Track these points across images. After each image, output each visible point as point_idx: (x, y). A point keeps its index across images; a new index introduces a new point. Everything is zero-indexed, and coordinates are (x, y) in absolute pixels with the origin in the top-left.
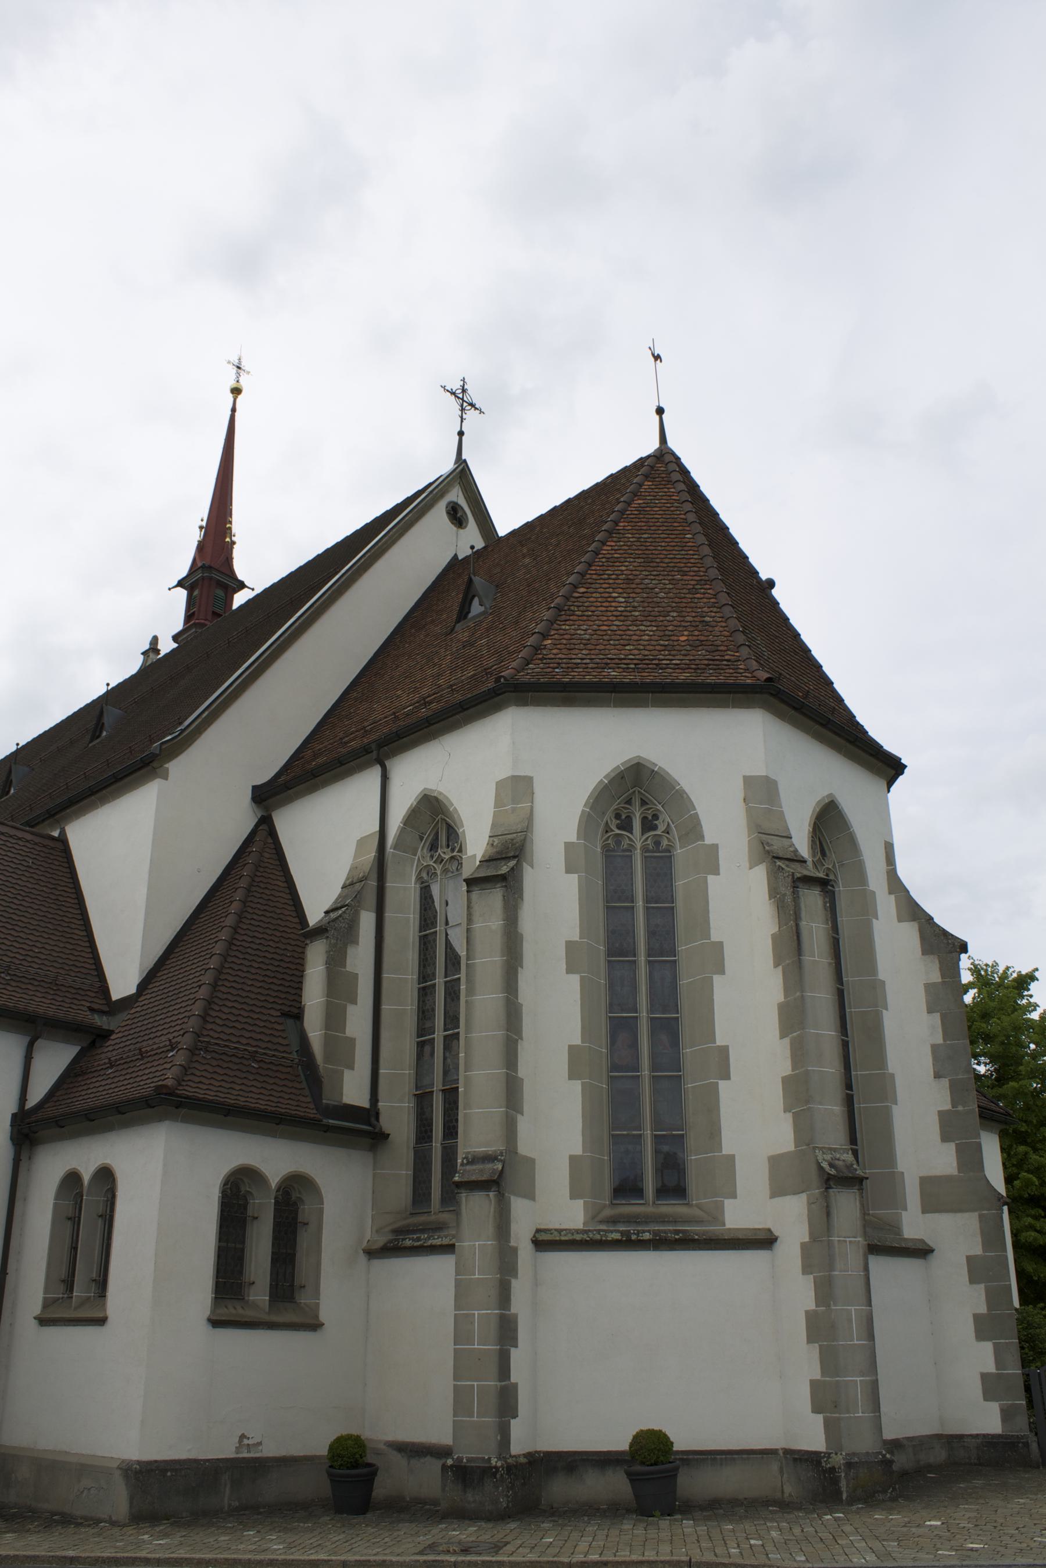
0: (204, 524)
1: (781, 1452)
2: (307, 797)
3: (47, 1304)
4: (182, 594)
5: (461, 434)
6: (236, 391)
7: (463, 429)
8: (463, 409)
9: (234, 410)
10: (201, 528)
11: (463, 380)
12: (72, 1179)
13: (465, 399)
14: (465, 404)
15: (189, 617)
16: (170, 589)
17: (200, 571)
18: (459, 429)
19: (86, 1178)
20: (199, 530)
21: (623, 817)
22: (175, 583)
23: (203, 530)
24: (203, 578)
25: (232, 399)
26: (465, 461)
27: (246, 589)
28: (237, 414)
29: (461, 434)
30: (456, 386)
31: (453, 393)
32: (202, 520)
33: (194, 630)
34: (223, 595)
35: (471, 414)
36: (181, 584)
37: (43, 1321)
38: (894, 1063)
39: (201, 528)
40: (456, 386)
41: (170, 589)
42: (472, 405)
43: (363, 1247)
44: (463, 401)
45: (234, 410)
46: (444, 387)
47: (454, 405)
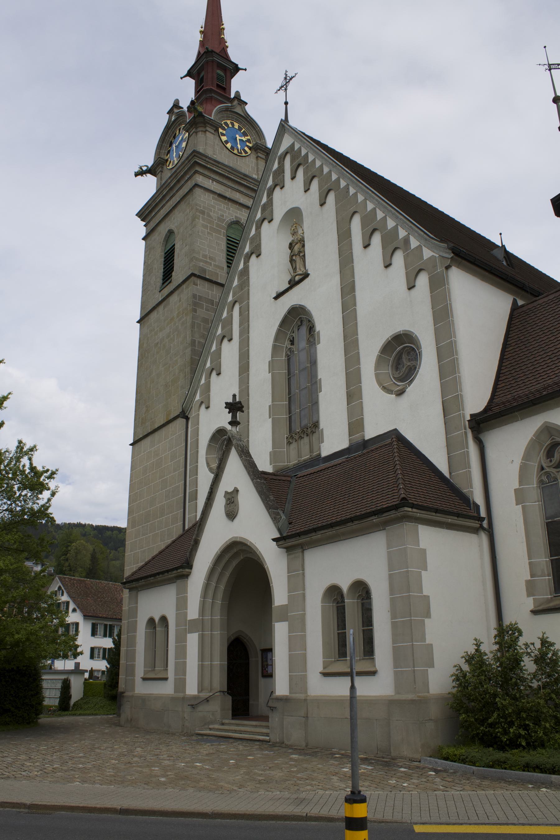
2: (503, 427)
3: (145, 672)
4: (191, 83)
5: (286, 103)
7: (287, 100)
8: (291, 79)
10: (201, 32)
12: (151, 621)
13: (285, 83)
14: (287, 81)
17: (204, 56)
18: (285, 101)
19: (157, 620)
21: (549, 460)
22: (186, 73)
24: (207, 62)
27: (240, 71)
29: (286, 103)
36: (190, 74)
37: (144, 679)
38: (269, 424)
44: (286, 83)
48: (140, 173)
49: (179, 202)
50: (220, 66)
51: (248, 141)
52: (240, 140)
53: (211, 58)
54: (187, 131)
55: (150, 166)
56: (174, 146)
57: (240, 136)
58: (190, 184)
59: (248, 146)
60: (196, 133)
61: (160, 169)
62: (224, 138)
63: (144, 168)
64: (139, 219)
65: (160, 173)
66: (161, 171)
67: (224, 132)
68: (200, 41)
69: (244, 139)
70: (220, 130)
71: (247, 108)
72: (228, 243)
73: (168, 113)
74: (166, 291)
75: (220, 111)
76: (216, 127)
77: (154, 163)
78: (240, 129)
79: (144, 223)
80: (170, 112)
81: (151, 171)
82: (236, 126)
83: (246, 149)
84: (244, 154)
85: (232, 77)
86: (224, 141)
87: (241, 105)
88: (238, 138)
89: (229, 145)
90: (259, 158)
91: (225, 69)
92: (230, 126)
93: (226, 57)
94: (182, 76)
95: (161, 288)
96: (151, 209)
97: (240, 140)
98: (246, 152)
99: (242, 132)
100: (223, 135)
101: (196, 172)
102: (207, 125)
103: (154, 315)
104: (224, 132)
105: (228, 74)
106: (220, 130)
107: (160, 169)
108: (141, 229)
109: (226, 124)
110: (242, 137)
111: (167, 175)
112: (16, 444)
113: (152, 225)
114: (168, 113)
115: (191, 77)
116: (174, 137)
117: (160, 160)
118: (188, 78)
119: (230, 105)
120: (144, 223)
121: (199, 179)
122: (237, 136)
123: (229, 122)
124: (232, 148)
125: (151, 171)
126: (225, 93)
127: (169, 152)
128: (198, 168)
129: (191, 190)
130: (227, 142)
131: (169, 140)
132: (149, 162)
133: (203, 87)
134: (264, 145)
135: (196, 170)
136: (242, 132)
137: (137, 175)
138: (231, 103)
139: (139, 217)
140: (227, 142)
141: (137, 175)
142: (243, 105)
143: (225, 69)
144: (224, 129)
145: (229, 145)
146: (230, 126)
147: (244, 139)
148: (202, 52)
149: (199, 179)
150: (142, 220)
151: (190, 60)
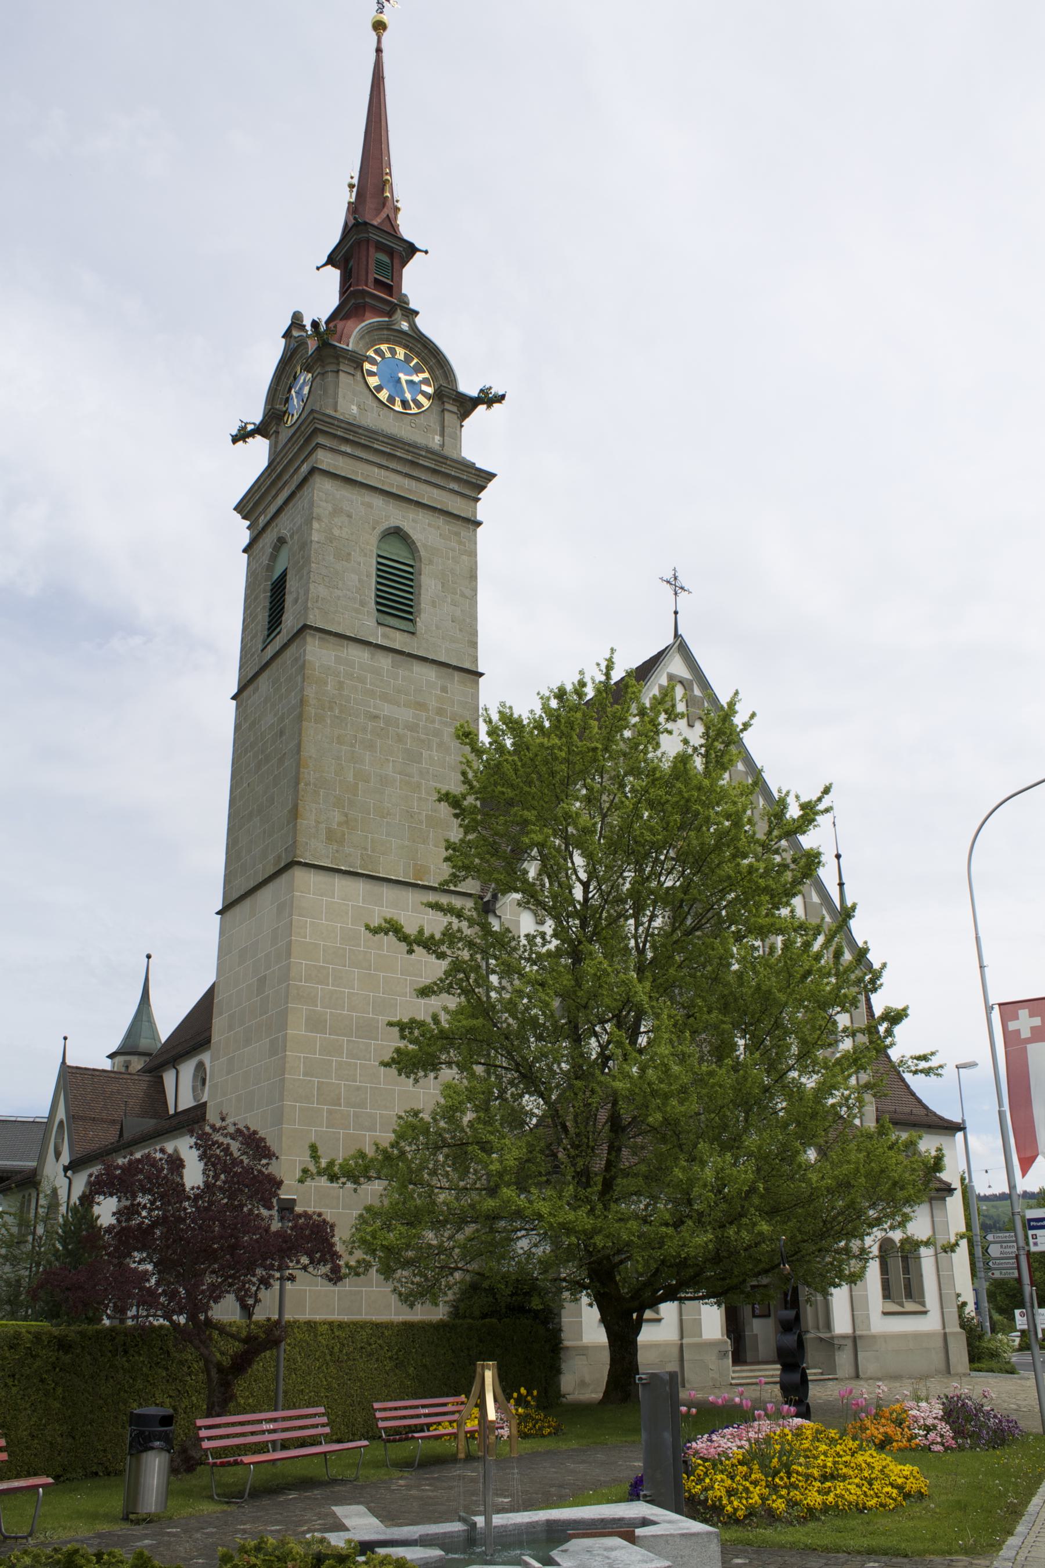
0: (355, 181)
1: (727, 1225)
4: (334, 275)
6: (379, 26)
9: (379, 50)
11: (675, 569)
15: (666, 1301)
16: (318, 268)
20: (348, 189)
22: (324, 259)
23: (355, 190)
25: (376, 38)
26: (681, 636)
28: (386, 56)
30: (669, 576)
31: (668, 582)
32: (352, 178)
33: (353, 301)
34: (388, 261)
35: (682, 595)
36: (331, 261)
39: (351, 186)
40: (669, 576)
41: (318, 268)
42: (682, 588)
43: (297, 1177)
45: (379, 50)
46: (661, 579)
47: (669, 590)
48: (242, 436)
49: (292, 495)
50: (380, 247)
51: (425, 381)
52: (407, 381)
53: (366, 235)
54: (309, 372)
55: (258, 422)
56: (293, 392)
57: (406, 374)
58: (305, 469)
59: (424, 393)
60: (323, 374)
61: (274, 429)
62: (373, 381)
63: (250, 427)
64: (239, 516)
65: (274, 436)
66: (275, 431)
67: (374, 369)
68: (349, 203)
69: (416, 378)
70: (367, 366)
71: (419, 321)
72: (379, 576)
73: (283, 337)
74: (270, 651)
75: (371, 330)
76: (357, 361)
77: (264, 417)
78: (408, 359)
79: (248, 523)
80: (287, 335)
81: (261, 430)
82: (401, 353)
83: (421, 398)
84: (415, 411)
85: (404, 264)
86: (374, 387)
87: (408, 317)
88: (403, 377)
89: (383, 395)
90: (446, 412)
91: (390, 252)
92: (388, 355)
93: (393, 233)
94: (319, 265)
95: (264, 642)
96: (265, 490)
97: (407, 381)
98: (419, 405)
99: (412, 365)
100: (371, 374)
101: (318, 445)
102: (341, 360)
103: (263, 681)
104: (374, 369)
105: (396, 261)
106: (367, 366)
107: (274, 429)
108: (241, 531)
109: (378, 352)
110: (411, 375)
111: (285, 435)
112: (501, 393)
113: (262, 521)
114: (283, 337)
115: (334, 266)
116: (295, 378)
117: (273, 413)
118: (329, 267)
119: (387, 319)
120: (248, 523)
121: (325, 459)
122: (401, 375)
123: (384, 347)
124: (391, 399)
125: (261, 430)
126: (391, 296)
127: (287, 400)
128: (321, 440)
129: (305, 480)
130: (379, 388)
131: (287, 383)
132: (256, 416)
133: (350, 286)
134: (454, 388)
135: (318, 444)
136: (412, 365)
137: (235, 440)
138: (390, 317)
139: (238, 512)
140: (379, 388)
141: (235, 440)
142: (411, 317)
143: (390, 252)
144: (373, 362)
145: (383, 395)
146: (388, 355)
147: (416, 378)
148: (350, 225)
149: (325, 459)
150: (244, 518)
151: (334, 237)
